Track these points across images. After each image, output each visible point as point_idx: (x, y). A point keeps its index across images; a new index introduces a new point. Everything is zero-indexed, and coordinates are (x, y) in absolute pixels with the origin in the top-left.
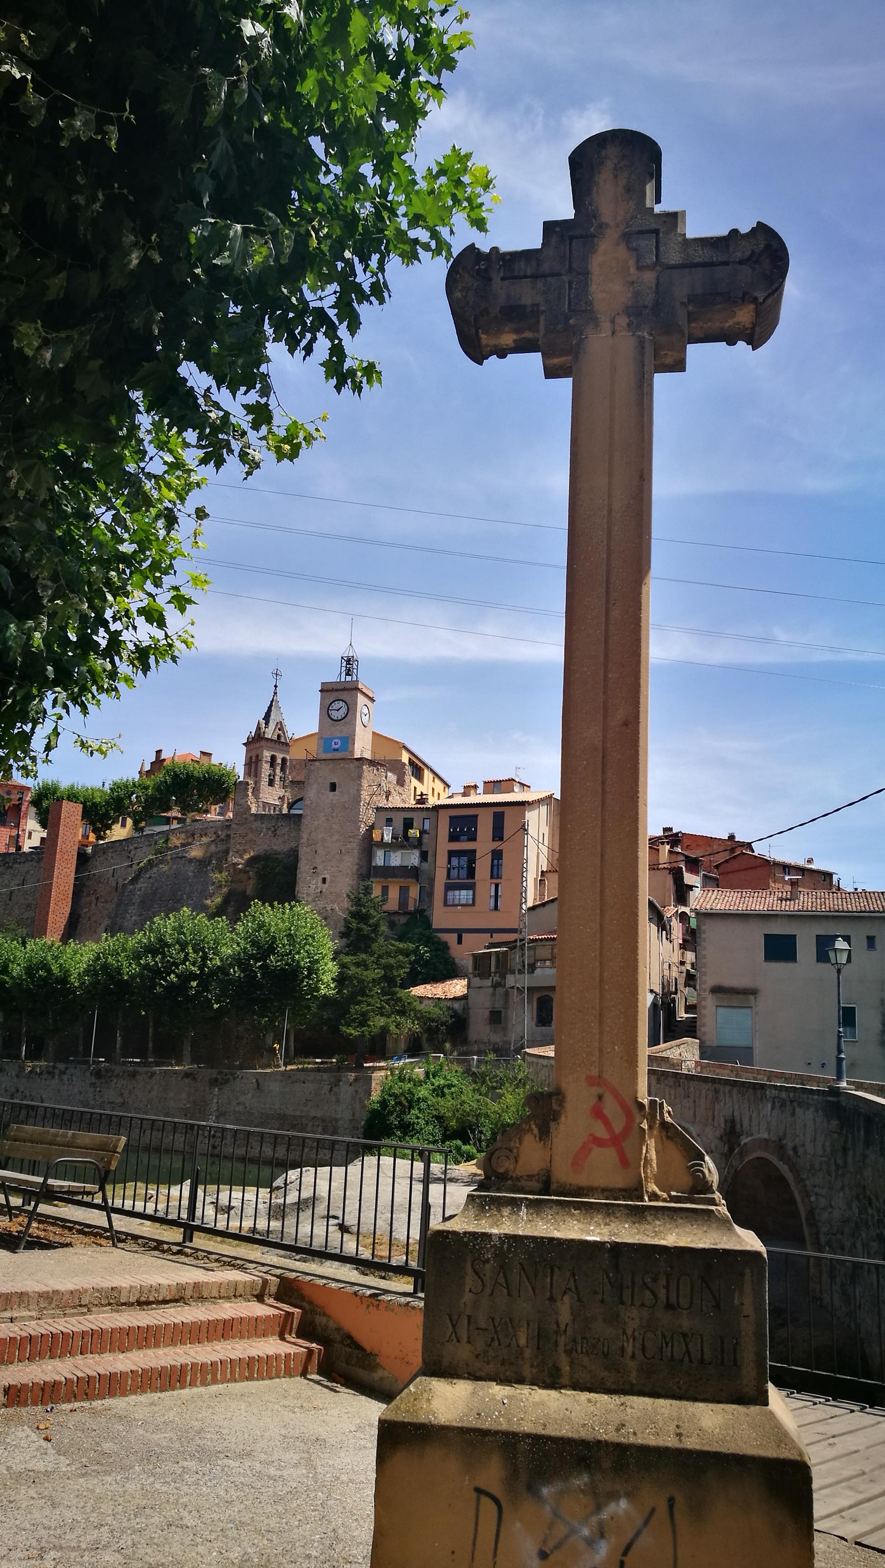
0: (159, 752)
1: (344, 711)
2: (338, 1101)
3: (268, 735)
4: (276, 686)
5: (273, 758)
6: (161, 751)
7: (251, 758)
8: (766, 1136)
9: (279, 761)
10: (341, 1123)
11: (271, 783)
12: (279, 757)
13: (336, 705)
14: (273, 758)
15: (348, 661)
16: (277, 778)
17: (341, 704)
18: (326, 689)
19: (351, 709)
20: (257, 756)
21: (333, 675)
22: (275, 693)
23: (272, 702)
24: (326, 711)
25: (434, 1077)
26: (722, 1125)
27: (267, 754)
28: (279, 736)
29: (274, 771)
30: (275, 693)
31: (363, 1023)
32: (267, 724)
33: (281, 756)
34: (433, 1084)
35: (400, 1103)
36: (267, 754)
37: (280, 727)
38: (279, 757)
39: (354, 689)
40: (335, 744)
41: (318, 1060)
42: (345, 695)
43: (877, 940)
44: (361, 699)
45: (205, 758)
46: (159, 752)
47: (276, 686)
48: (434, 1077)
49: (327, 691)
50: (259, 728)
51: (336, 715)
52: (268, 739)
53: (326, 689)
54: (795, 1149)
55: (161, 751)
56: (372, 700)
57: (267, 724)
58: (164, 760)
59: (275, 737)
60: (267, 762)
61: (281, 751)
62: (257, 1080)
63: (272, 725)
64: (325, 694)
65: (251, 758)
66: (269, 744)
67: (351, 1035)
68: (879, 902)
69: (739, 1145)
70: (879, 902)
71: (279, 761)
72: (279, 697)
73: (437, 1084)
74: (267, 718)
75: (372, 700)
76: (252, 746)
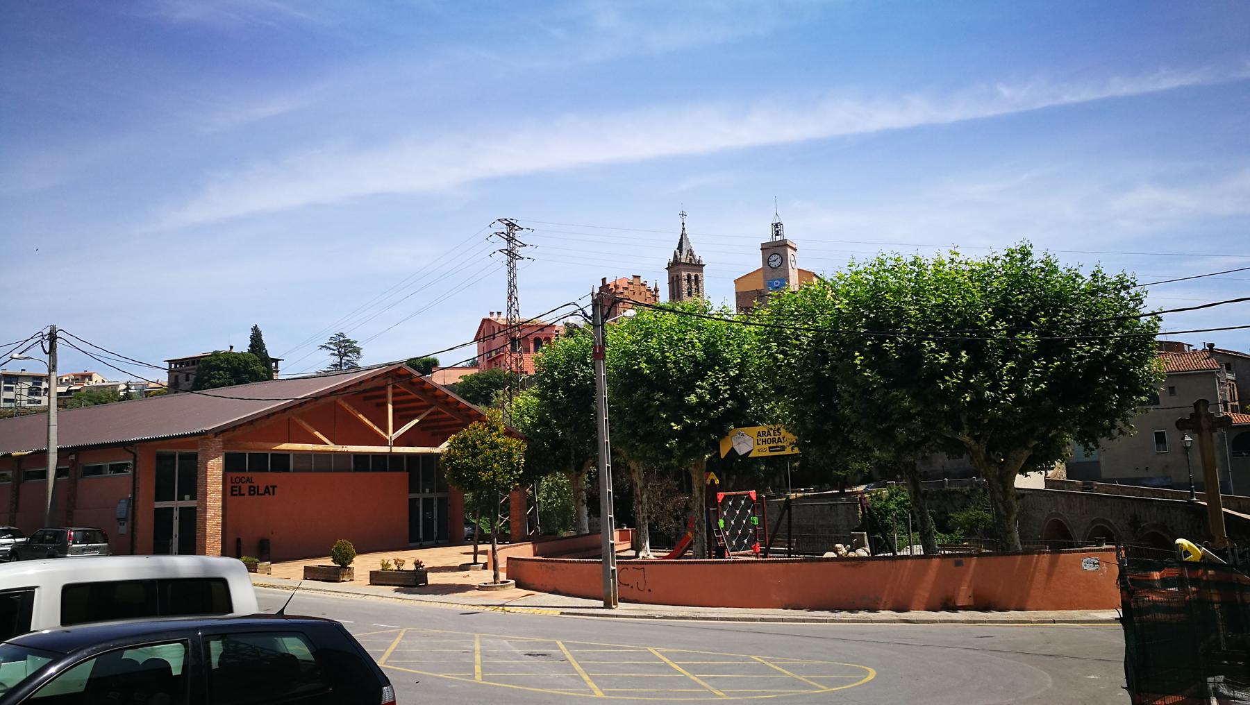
0: (604, 280)
1: (779, 261)
2: (837, 515)
3: (683, 261)
4: (683, 224)
5: (689, 276)
6: (605, 278)
7: (673, 278)
8: (1155, 522)
9: (693, 278)
10: (841, 527)
11: (690, 294)
12: (693, 274)
13: (773, 258)
14: (689, 276)
15: (777, 225)
16: (693, 290)
17: (777, 256)
18: (765, 248)
19: (784, 259)
20: (677, 276)
21: (768, 237)
22: (684, 229)
23: (682, 235)
24: (766, 261)
25: (896, 497)
26: (1130, 518)
27: (684, 274)
28: (690, 259)
29: (690, 285)
30: (684, 229)
31: (846, 468)
32: (681, 252)
33: (694, 274)
34: (896, 500)
35: (880, 514)
36: (684, 274)
37: (690, 252)
38: (693, 274)
39: (784, 245)
40: (777, 284)
41: (803, 489)
42: (779, 250)
43: (1176, 389)
44: (789, 250)
45: (637, 280)
46: (604, 280)
47: (683, 224)
48: (896, 497)
49: (765, 249)
50: (675, 256)
51: (773, 264)
52: (683, 263)
53: (765, 248)
54: (1172, 528)
55: (605, 278)
56: (795, 250)
57: (681, 252)
58: (609, 285)
59: (688, 261)
60: (685, 280)
61: (693, 271)
62: (779, 506)
63: (685, 252)
64: (765, 251)
65: (673, 278)
66: (685, 267)
67: (840, 475)
68: (1177, 364)
69: (1140, 527)
70: (1173, 362)
71: (693, 278)
72: (686, 232)
73: (899, 500)
74: (680, 247)
75: (795, 250)
76: (672, 270)
